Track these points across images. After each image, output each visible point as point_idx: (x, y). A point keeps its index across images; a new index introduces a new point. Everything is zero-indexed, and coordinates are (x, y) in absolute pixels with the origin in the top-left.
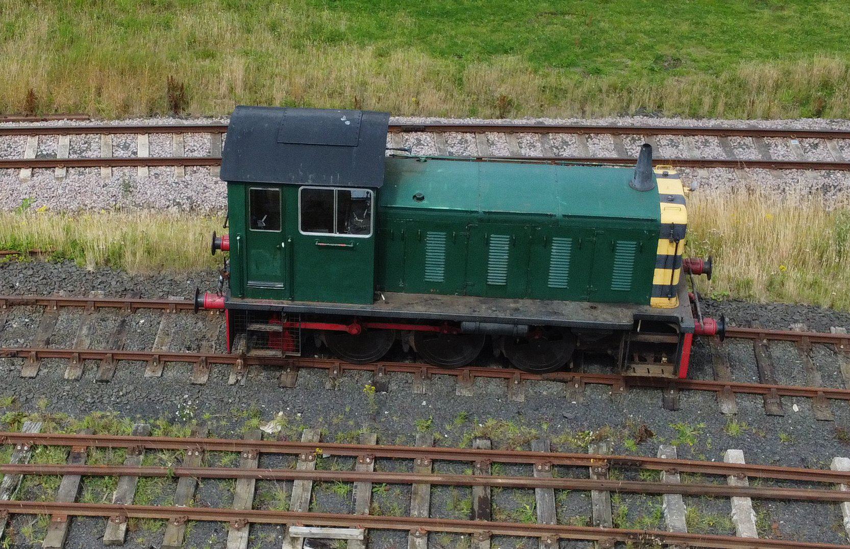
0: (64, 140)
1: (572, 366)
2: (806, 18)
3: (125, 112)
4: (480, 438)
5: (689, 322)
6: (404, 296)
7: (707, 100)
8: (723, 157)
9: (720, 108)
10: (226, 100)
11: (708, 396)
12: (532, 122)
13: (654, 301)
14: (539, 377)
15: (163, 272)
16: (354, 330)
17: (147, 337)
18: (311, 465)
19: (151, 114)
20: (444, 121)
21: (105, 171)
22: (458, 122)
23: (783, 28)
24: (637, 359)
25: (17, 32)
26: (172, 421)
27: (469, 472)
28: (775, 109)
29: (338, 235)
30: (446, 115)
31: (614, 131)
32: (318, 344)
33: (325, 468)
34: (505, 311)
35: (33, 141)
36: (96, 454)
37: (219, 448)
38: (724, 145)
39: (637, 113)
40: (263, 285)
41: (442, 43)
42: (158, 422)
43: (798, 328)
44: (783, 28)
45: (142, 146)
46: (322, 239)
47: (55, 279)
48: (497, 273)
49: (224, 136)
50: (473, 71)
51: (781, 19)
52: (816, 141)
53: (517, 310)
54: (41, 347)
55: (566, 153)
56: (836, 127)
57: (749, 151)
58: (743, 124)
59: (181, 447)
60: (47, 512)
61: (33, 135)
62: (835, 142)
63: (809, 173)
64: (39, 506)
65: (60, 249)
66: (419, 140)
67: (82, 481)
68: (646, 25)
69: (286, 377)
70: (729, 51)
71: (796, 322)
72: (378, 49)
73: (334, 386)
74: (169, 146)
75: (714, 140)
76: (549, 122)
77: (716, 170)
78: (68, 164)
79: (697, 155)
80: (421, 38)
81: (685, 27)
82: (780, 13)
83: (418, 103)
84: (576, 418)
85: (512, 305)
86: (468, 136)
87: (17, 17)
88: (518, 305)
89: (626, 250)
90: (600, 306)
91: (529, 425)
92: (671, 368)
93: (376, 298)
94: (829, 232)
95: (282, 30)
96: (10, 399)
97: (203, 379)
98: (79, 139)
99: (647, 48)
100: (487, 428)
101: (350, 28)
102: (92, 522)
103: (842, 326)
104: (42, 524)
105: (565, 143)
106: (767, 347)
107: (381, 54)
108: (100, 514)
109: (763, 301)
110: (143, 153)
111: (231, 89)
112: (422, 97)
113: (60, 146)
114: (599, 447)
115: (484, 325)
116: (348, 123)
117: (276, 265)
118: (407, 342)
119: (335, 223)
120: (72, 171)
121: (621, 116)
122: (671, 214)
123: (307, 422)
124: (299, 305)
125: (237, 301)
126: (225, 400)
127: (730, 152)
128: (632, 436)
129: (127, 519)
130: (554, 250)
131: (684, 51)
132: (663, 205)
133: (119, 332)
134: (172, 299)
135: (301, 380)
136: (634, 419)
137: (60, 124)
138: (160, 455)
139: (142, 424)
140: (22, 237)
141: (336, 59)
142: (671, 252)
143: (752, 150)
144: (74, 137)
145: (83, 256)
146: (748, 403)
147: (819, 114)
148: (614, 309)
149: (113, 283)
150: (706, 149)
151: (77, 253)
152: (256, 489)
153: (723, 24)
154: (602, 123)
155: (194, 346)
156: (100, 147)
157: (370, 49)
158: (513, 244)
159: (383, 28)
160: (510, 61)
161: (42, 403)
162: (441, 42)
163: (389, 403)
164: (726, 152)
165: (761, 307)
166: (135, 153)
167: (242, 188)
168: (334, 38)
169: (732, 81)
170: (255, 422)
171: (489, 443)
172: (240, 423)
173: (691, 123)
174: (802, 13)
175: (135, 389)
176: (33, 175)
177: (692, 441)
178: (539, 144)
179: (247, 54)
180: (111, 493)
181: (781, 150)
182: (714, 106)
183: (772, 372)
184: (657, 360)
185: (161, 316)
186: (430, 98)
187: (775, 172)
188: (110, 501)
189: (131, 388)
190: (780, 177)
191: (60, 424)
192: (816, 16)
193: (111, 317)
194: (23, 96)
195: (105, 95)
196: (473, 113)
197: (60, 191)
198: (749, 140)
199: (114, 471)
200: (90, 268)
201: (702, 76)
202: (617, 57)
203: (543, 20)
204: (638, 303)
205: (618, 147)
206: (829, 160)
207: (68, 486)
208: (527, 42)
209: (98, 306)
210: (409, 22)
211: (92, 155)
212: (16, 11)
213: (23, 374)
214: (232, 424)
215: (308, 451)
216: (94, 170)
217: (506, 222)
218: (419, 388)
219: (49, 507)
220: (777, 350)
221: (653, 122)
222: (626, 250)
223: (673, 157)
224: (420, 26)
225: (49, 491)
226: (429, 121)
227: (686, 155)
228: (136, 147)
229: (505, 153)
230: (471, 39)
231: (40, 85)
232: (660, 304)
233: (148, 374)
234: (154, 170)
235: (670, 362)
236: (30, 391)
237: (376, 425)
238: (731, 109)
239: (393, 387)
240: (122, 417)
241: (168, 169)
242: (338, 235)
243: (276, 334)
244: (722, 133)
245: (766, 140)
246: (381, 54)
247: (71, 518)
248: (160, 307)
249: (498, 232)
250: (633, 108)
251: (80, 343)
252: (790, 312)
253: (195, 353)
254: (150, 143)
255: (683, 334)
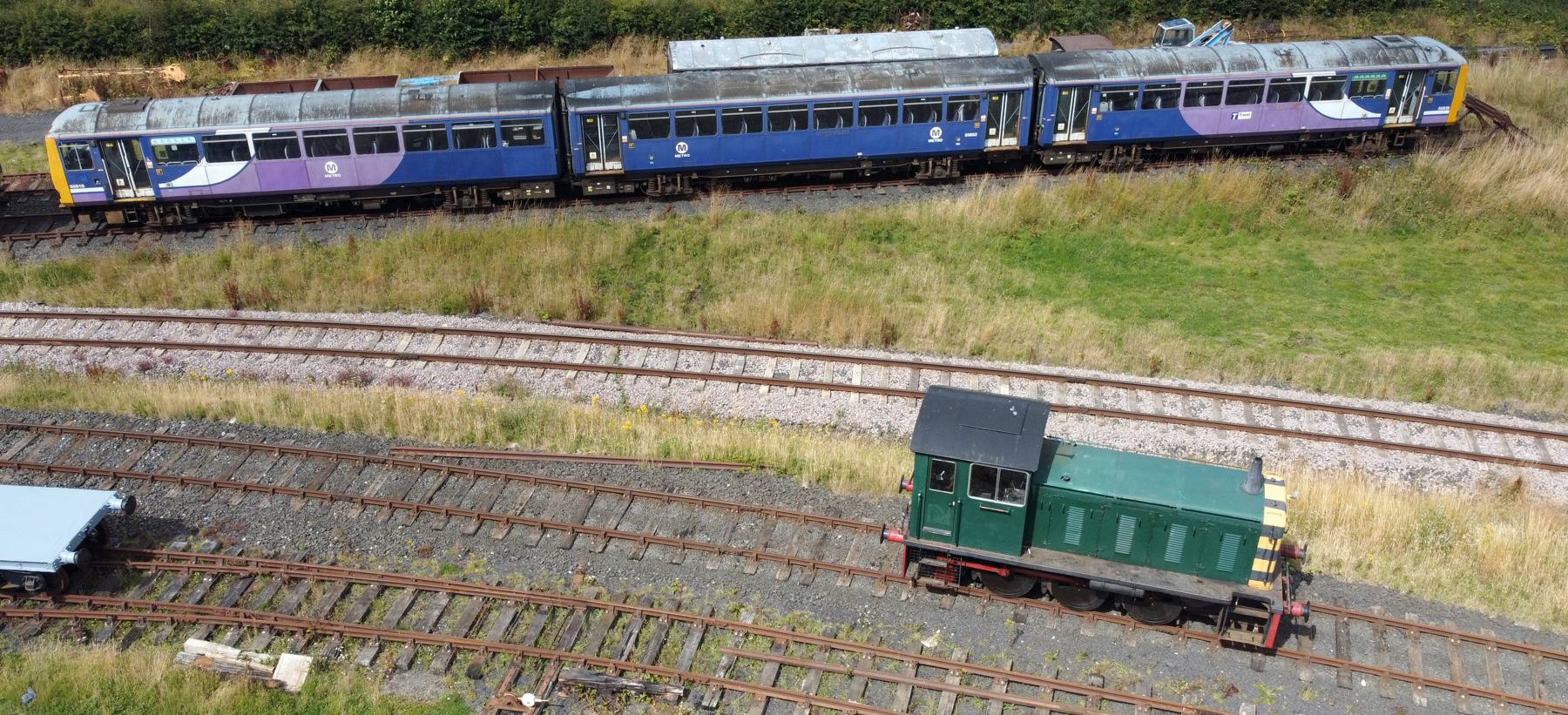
0: (796, 363)
1: (1178, 622)
2: (1429, 310)
3: (846, 342)
4: (1095, 675)
5: (1278, 606)
6: (1046, 552)
7: (1330, 378)
8: (1338, 433)
9: (1341, 385)
10: (927, 340)
11: (1290, 663)
12: (1177, 383)
13: (1252, 582)
14: (1151, 628)
15: (860, 495)
16: (1004, 573)
17: (842, 550)
18: (957, 680)
19: (866, 346)
20: (1103, 375)
21: (825, 393)
22: (1114, 377)
23: (1407, 316)
24: (1233, 625)
25: (770, 267)
26: (853, 627)
27: (1082, 703)
28: (1390, 392)
29: (998, 502)
30: (1104, 369)
31: (1247, 399)
32: (974, 578)
33: (968, 684)
34: (1127, 575)
35: (772, 361)
36: (792, 647)
37: (887, 655)
38: (1339, 421)
39: (1267, 384)
40: (934, 531)
41: (1108, 305)
42: (843, 626)
43: (1376, 610)
44: (1407, 316)
45: (856, 374)
46: (985, 503)
47: (777, 492)
48: (1124, 544)
49: (920, 402)
50: (1132, 333)
51: (1406, 308)
52: (1422, 425)
53: (1136, 576)
54: (761, 549)
55: (1202, 416)
56: (1442, 415)
57: (1360, 428)
58: (1358, 403)
59: (859, 651)
60: (752, 691)
61: (773, 357)
62: (1439, 428)
63: (1411, 455)
64: (747, 686)
65: (784, 466)
66: (1079, 391)
67: (780, 668)
68: (1286, 304)
69: (946, 600)
70: (1355, 334)
71: (1375, 604)
72: (1055, 305)
73: (983, 613)
74: (877, 376)
75: (1331, 416)
76: (1191, 385)
77: (1330, 444)
78: (797, 384)
79: (1315, 428)
80: (1093, 299)
81: (1319, 308)
82: (1406, 302)
83: (1082, 357)
84: (1176, 668)
85: (1133, 572)
86: (1121, 391)
87: (772, 254)
88: (1139, 572)
89: (1231, 542)
90: (1206, 581)
91: (1136, 668)
92: (1260, 637)
93: (1023, 551)
94: (1417, 526)
95: (978, 283)
96: (733, 591)
97: (881, 593)
98: (808, 363)
99: (1285, 325)
100: (1102, 666)
101: (1034, 285)
102: (785, 704)
103: (1415, 613)
104: (747, 700)
105: (1203, 406)
106: (1347, 624)
107: (1057, 311)
108: (791, 699)
109: (1350, 580)
110: (856, 382)
111: (933, 331)
112: (1086, 352)
113: (792, 368)
114: (1191, 697)
115: (1108, 585)
116: (1015, 413)
117: (948, 517)
118: (1045, 586)
119: (997, 490)
120: (799, 390)
121: (1255, 384)
122: (1273, 518)
123: (958, 643)
124: (962, 550)
125: (913, 541)
126: (897, 613)
127: (1343, 427)
128: (1220, 689)
129: (811, 706)
130: (1173, 532)
131: (1316, 331)
132: (1267, 509)
133: (821, 544)
134: (864, 520)
135: (957, 604)
136: (1226, 675)
137: (795, 348)
138: (841, 654)
139: (830, 625)
140: (756, 454)
141: (1019, 313)
142: (1270, 547)
143: (1364, 428)
144: (804, 361)
145: (800, 474)
146: (1322, 673)
147: (1429, 399)
148: (1218, 585)
149: (821, 500)
150: (1324, 423)
151: (796, 471)
152: (912, 694)
153: (1354, 308)
154: (1237, 390)
155: (877, 563)
156: (824, 371)
157: (1049, 307)
158: (1139, 524)
159: (1061, 287)
160: (1165, 326)
161: (756, 597)
162: (1108, 305)
163: (1026, 634)
164: (1341, 427)
165: (1348, 585)
166: (850, 380)
167: (926, 458)
168: (1020, 294)
169: (1354, 362)
170: (917, 636)
171: (1101, 680)
172: (905, 635)
173: (1314, 398)
174: (1426, 303)
175: (829, 594)
176: (769, 391)
177: (1271, 701)
178: (1179, 404)
179: (947, 300)
180: (801, 682)
181: (1391, 431)
182: (1335, 383)
183: (1349, 648)
184: (1250, 629)
185: (854, 534)
186: (1094, 353)
187: (1381, 452)
188: (800, 687)
189: (825, 593)
190: (1385, 456)
191: (768, 617)
192: (1439, 307)
193: (816, 529)
194: (768, 322)
195: (831, 327)
196: (1127, 369)
197: (789, 407)
198: (1362, 419)
199: (805, 664)
200: (805, 485)
201: (1328, 356)
202: (1257, 331)
203: (1197, 291)
204: (1238, 582)
205: (1248, 415)
206: (1431, 445)
207: (770, 670)
208: (1181, 310)
209: (807, 520)
210: (1084, 284)
211: (816, 378)
212: (771, 250)
213: (745, 571)
214: (900, 635)
215: (956, 668)
216: (817, 392)
217: (1133, 507)
218: (1052, 623)
219: (754, 688)
220: (1356, 628)
221: (1281, 394)
222: (1231, 542)
223: (1294, 428)
224: (1093, 289)
225: (755, 673)
226: (1090, 374)
227: (1305, 428)
228: (851, 374)
229: (1150, 410)
230: (1134, 304)
231: (782, 313)
232: (1256, 587)
233: (839, 583)
234: (864, 396)
235: (1261, 631)
236: (748, 586)
237: (1012, 651)
238: (1350, 389)
239: (1030, 620)
240: (816, 618)
241: (875, 396)
242: (998, 502)
243: (942, 568)
244: (1340, 410)
245: (1378, 420)
246: (1057, 311)
247: (769, 698)
248: (854, 526)
249: (1129, 514)
250: (1265, 378)
251: (790, 549)
252: (1371, 593)
253: (877, 569)
254: (863, 372)
255: (1272, 614)
